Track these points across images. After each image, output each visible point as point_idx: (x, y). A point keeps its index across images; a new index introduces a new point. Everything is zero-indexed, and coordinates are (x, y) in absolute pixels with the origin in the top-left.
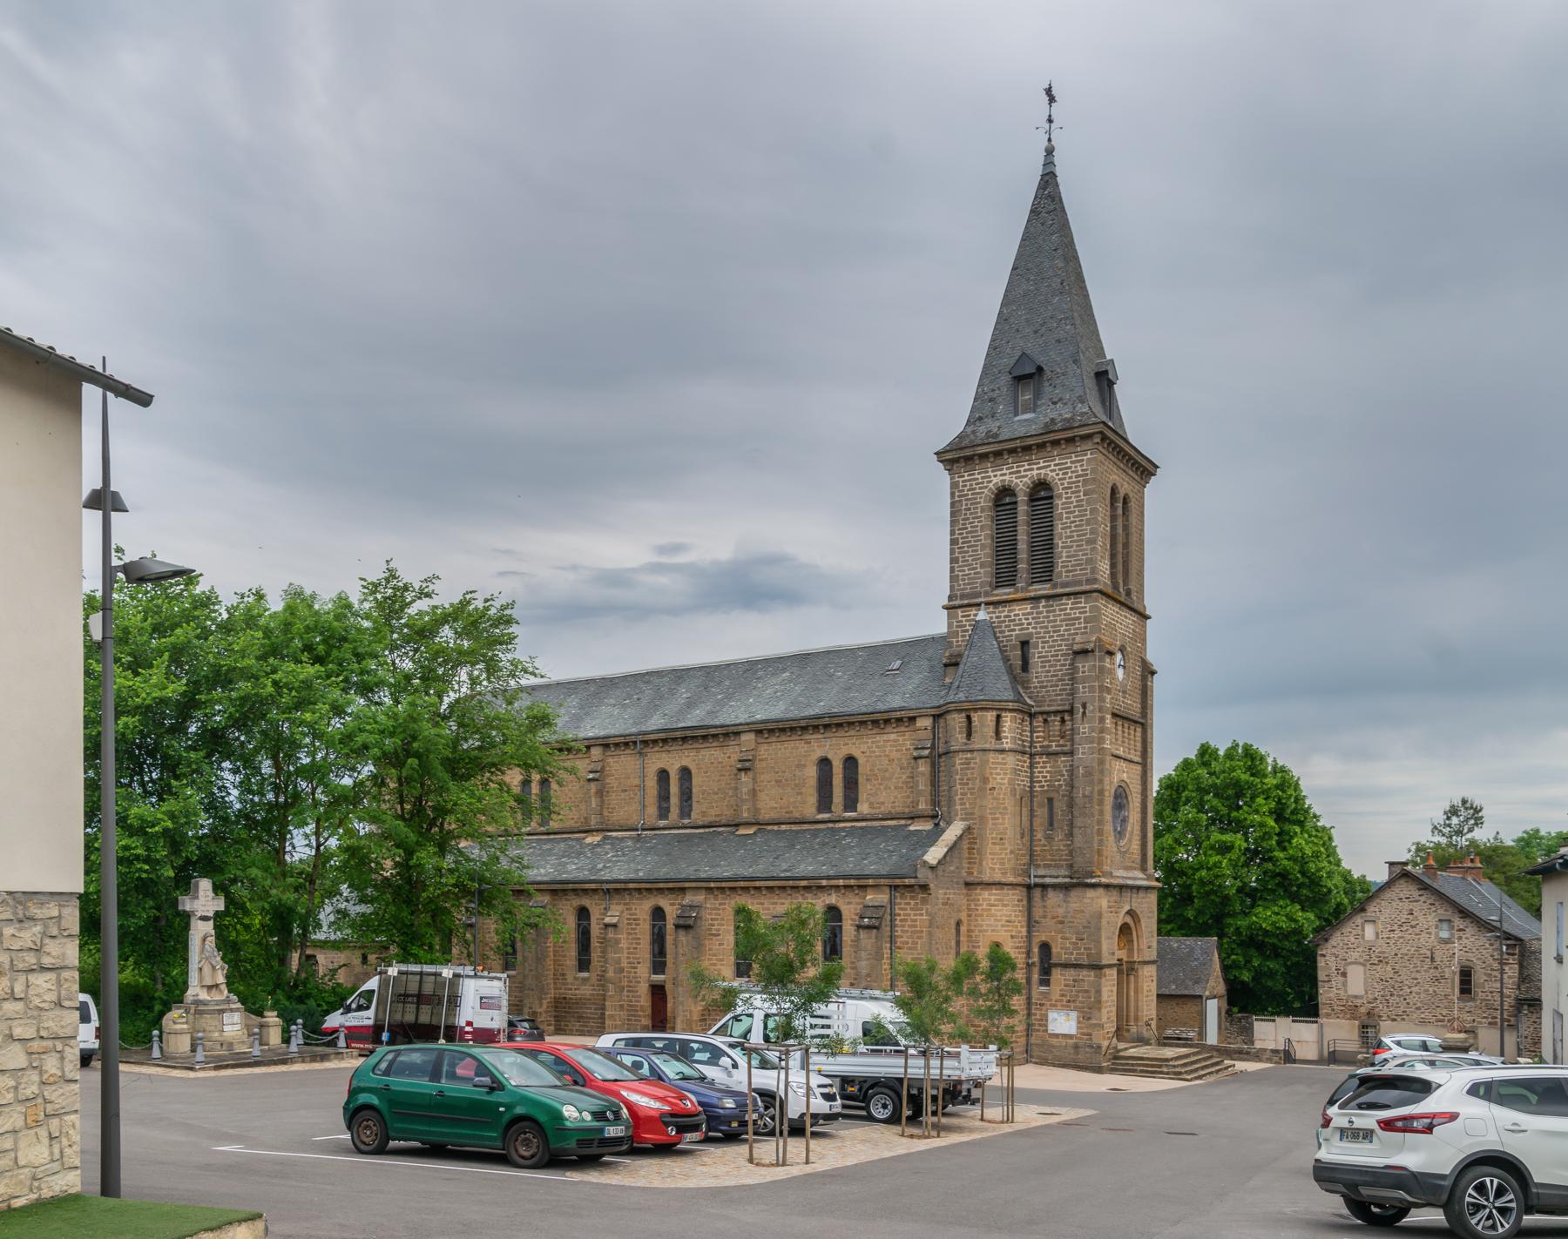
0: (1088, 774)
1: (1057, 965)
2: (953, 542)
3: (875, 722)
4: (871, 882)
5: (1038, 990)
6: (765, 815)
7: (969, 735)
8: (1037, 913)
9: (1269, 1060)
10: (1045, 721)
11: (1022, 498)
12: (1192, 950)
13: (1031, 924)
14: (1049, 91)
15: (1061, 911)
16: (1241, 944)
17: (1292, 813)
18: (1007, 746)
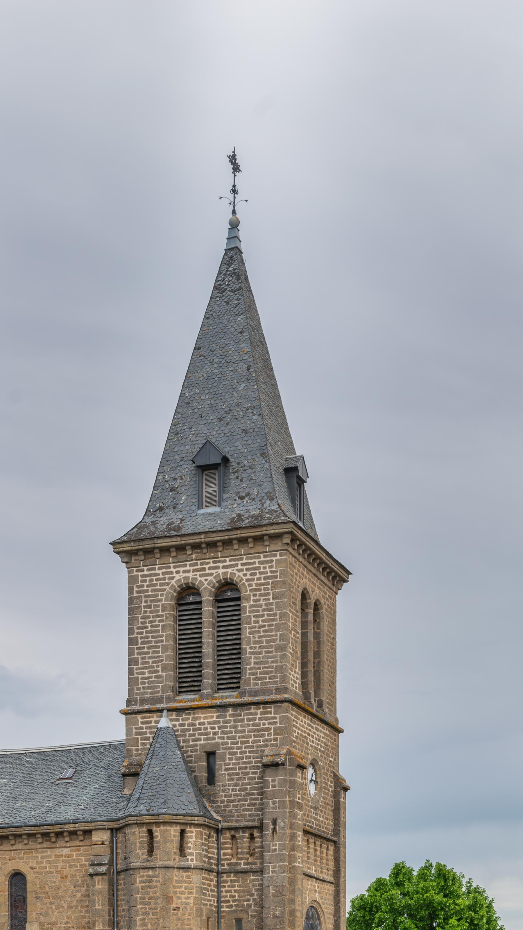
0: (279, 893)
2: (132, 641)
10: (233, 837)
11: (207, 598)
14: (233, 159)
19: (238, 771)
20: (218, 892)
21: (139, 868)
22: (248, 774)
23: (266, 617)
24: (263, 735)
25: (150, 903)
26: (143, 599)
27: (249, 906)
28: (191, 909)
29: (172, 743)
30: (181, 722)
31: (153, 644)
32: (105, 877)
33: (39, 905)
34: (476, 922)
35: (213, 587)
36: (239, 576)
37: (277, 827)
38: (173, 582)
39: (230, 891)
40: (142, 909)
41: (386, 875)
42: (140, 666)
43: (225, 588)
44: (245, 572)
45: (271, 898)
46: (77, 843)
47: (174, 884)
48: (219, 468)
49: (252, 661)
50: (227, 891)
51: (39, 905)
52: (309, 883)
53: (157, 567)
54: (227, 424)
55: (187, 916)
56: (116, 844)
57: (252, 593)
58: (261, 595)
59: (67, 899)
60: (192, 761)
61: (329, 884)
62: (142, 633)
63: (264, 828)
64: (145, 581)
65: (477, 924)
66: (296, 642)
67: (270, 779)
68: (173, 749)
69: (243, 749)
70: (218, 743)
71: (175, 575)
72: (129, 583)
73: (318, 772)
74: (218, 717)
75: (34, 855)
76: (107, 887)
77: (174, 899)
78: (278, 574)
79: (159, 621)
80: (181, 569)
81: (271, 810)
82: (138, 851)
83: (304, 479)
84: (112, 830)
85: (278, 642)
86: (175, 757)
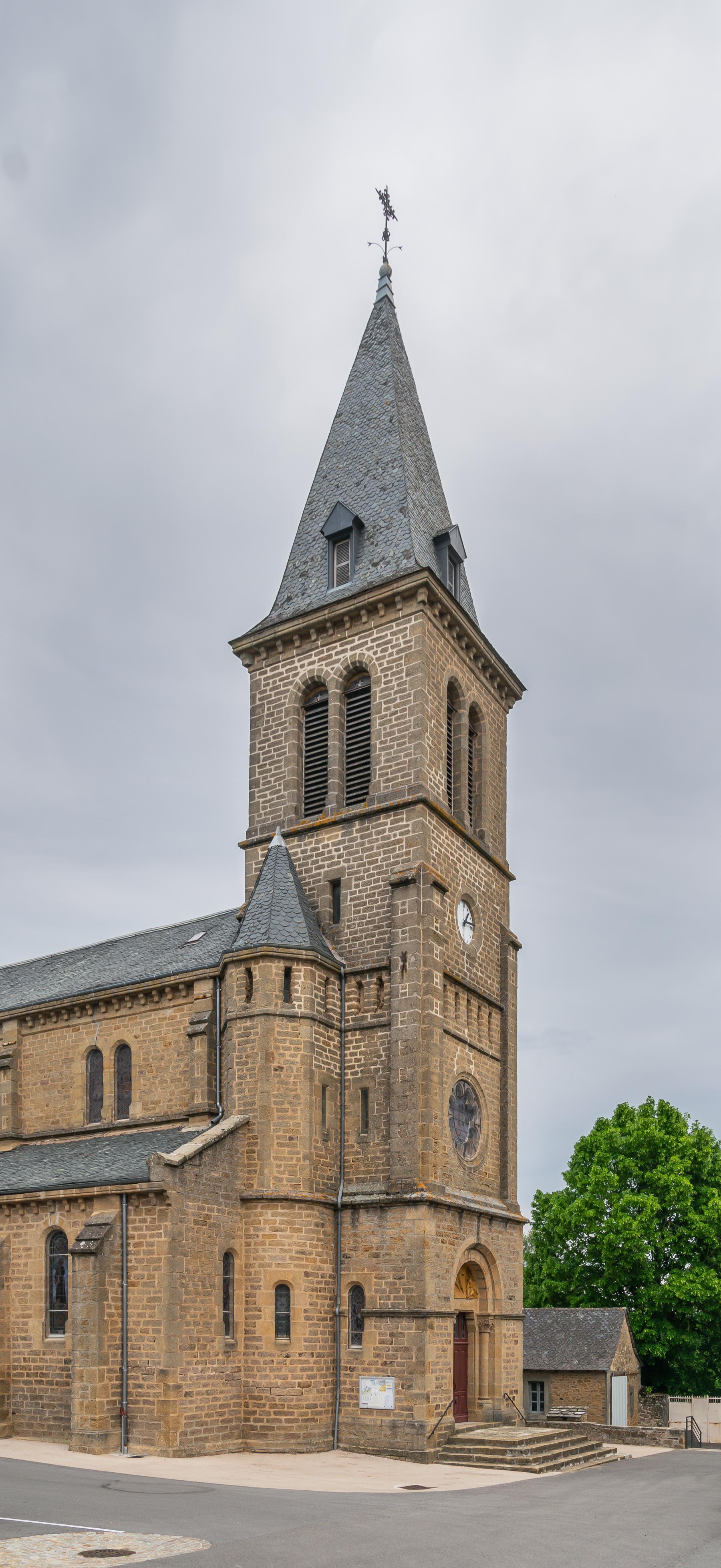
0: (408, 1050)
1: (371, 1314)
2: (253, 760)
3: (148, 994)
4: (96, 1191)
5: (347, 1350)
6: (29, 1129)
7: (249, 998)
8: (347, 1243)
9: (668, 1443)
10: (360, 986)
11: (334, 691)
12: (599, 1322)
13: (339, 1259)
14: (384, 197)
15: (375, 1240)
16: (655, 1316)
17: (710, 1174)
18: (298, 1011)
19: (365, 900)
20: (341, 1056)
21: (235, 1019)
22: (376, 901)
23: (398, 701)
24: (394, 850)
25: (247, 1062)
26: (266, 707)
27: (377, 1070)
28: (298, 1070)
29: (284, 865)
30: (303, 848)
31: (276, 758)
32: (205, 1037)
33: (142, 1082)
34: (700, 1160)
35: (340, 676)
36: (369, 656)
37: (407, 964)
38: (297, 679)
39: (355, 1054)
40: (239, 1070)
41: (609, 1116)
42: (262, 787)
43: (356, 678)
44: (375, 649)
45: (400, 1057)
46: (181, 1001)
47: (276, 1036)
49: (383, 759)
50: (352, 1054)
51: (142, 1082)
52: (459, 1048)
53: (280, 664)
54: (365, 487)
55: (292, 1079)
56: (220, 996)
57: (383, 675)
58: (393, 674)
59: (171, 1071)
60: (314, 894)
62: (264, 747)
63: (392, 967)
64: (268, 684)
65: (701, 1163)
66: (439, 737)
67: (399, 902)
68: (284, 872)
69: (372, 872)
70: (343, 868)
71: (299, 670)
72: (251, 691)
73: (475, 916)
74: (343, 835)
75: (139, 1020)
76: (206, 1049)
77: (276, 1056)
78: (413, 643)
79: (283, 730)
80: (306, 662)
81: (400, 942)
82: (235, 997)
84: (214, 978)
85: (412, 730)
86: (286, 880)
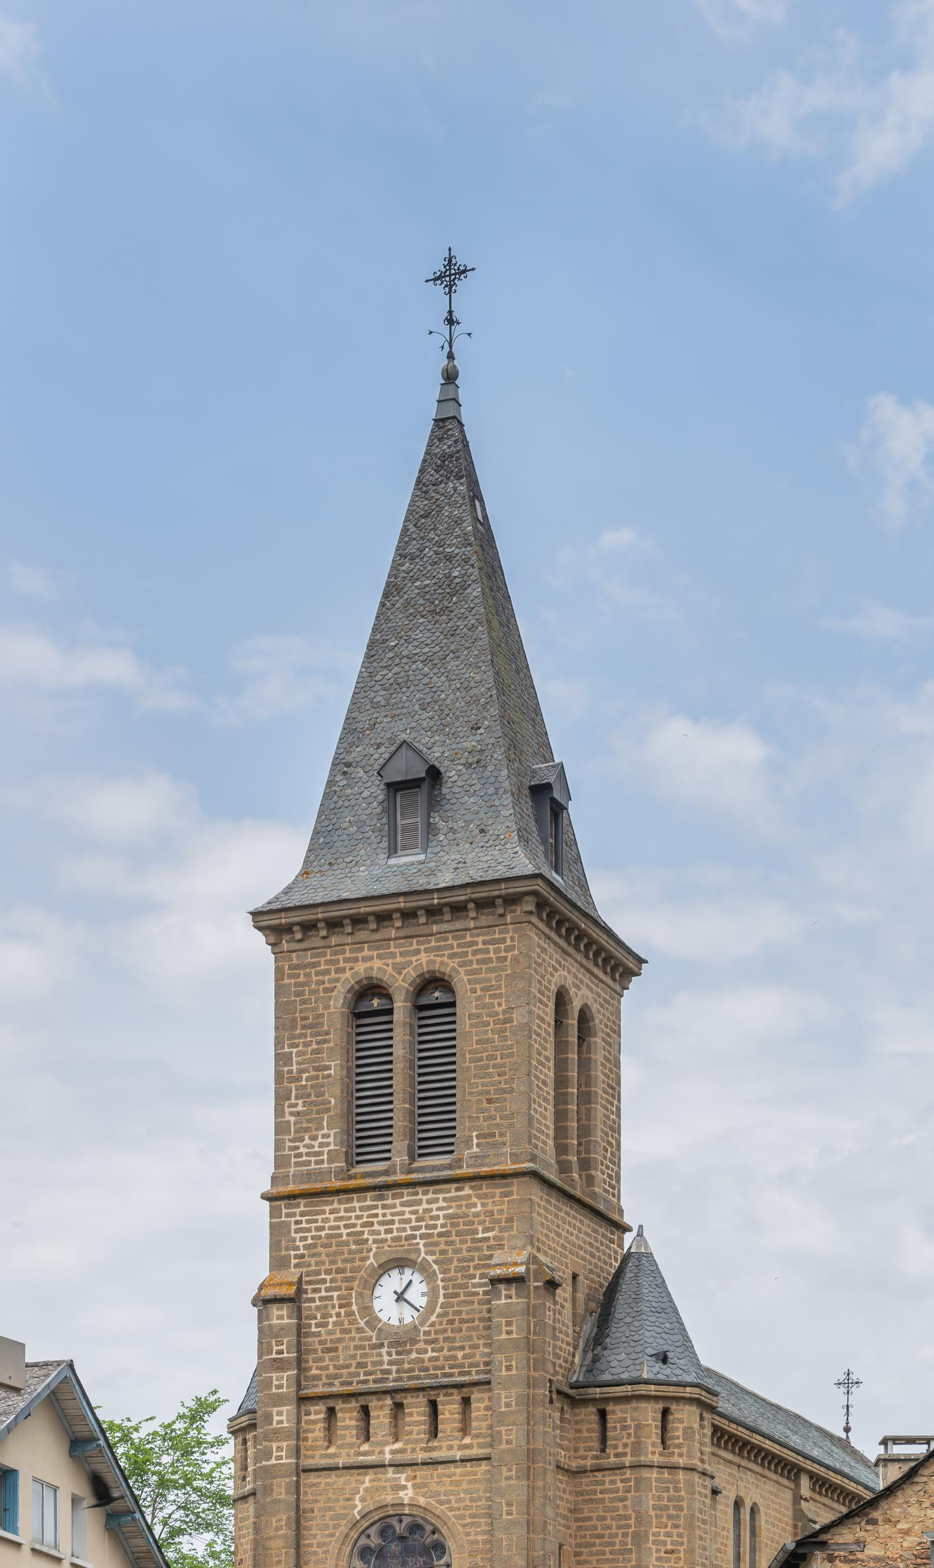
48: (422, 785)
61: (425, 1467)
83: (563, 803)
